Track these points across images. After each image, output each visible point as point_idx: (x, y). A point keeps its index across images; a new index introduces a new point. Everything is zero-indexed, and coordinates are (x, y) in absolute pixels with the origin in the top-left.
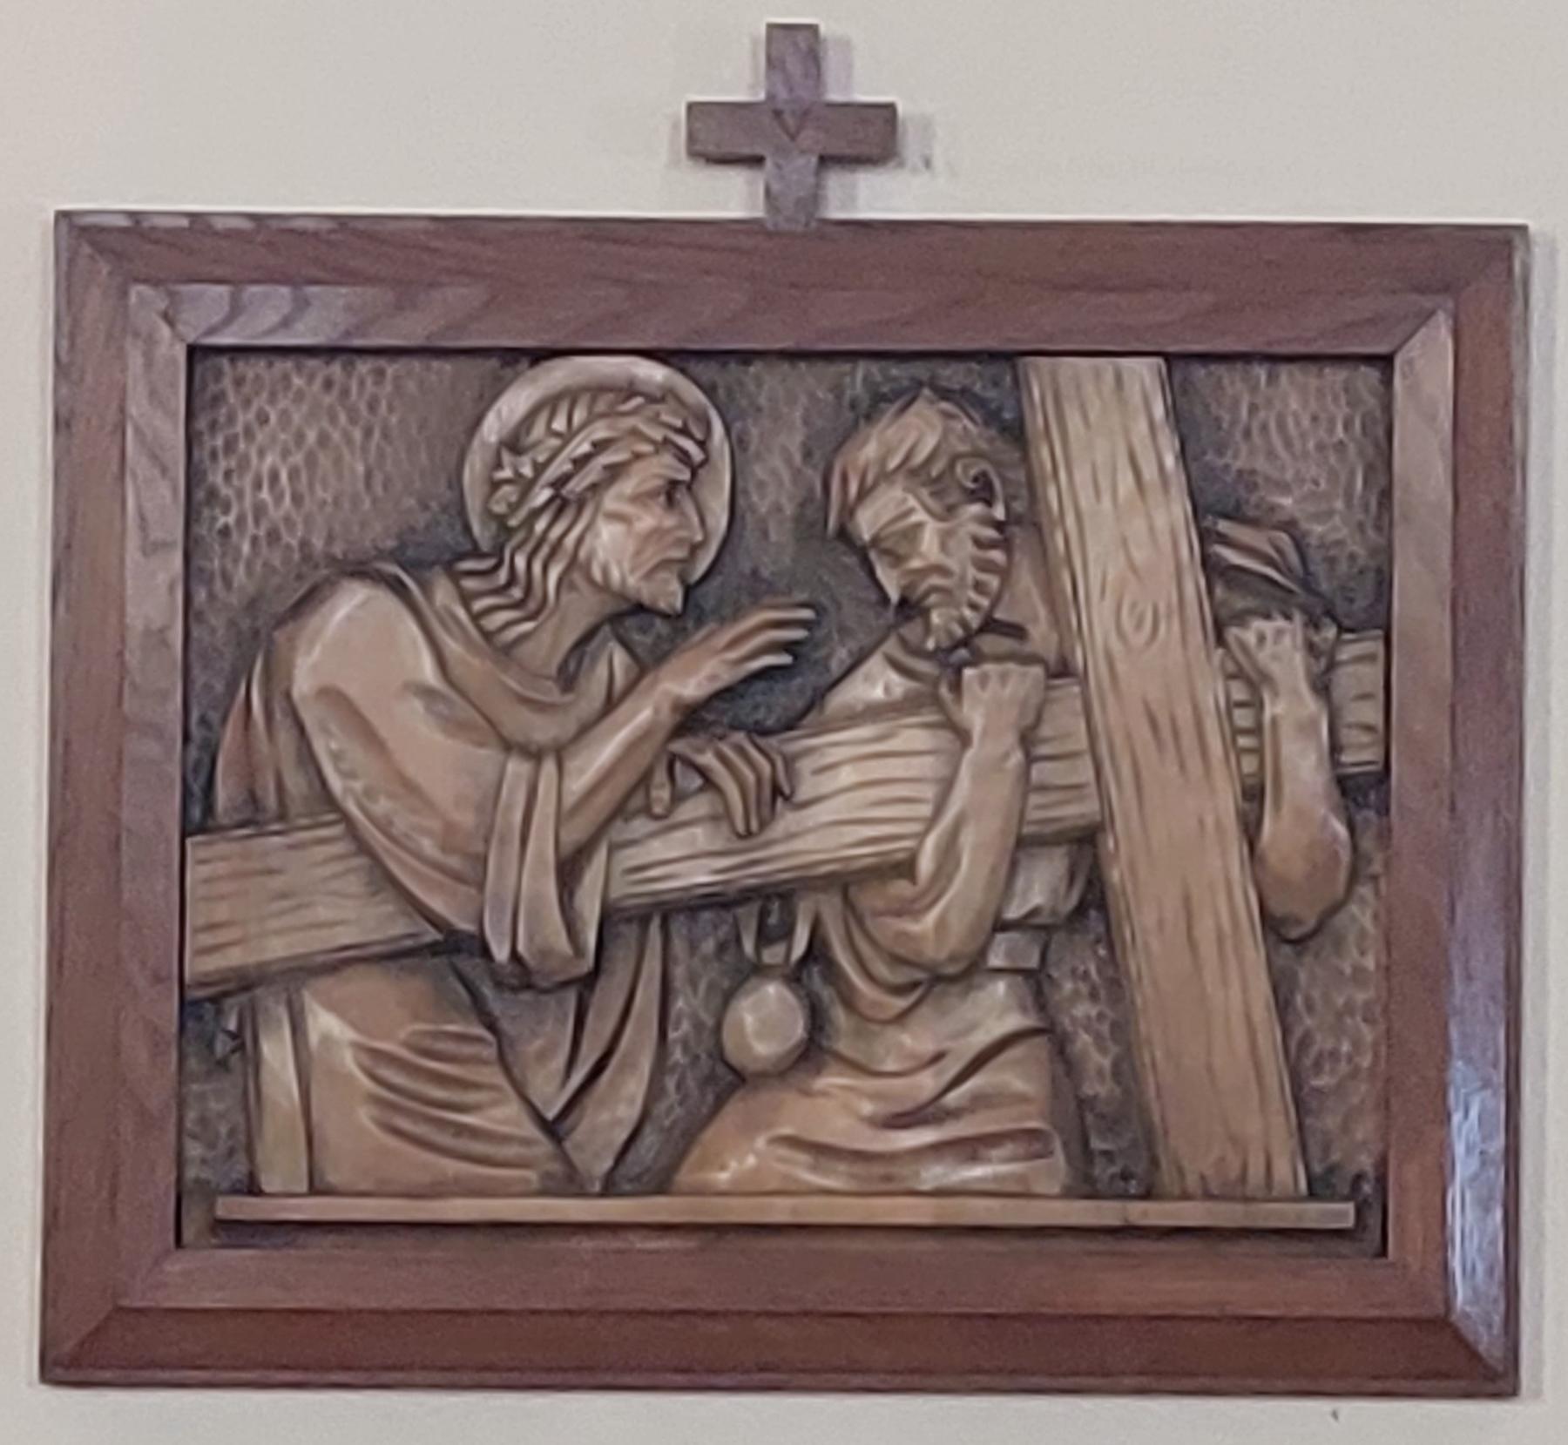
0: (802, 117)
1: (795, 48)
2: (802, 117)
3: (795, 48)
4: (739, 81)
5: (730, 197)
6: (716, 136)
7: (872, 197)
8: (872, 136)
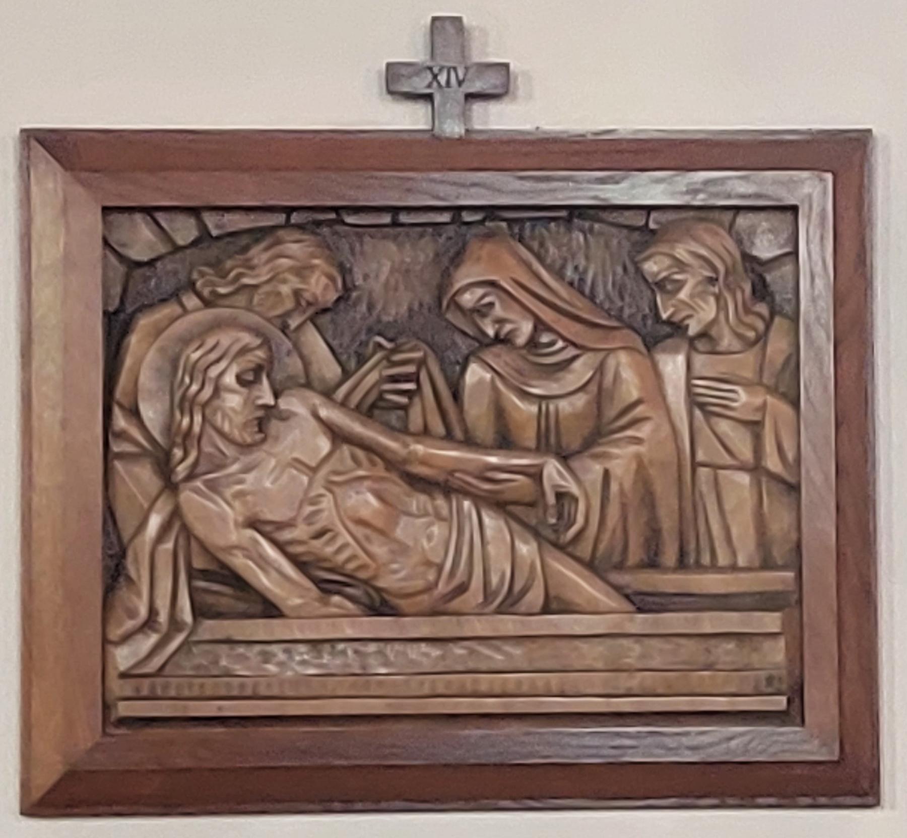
0: (449, 67)
1: (446, 30)
2: (449, 67)
3: (446, 30)
4: (413, 51)
5: (409, 118)
6: (396, 82)
7: (496, 118)
8: (499, 84)
